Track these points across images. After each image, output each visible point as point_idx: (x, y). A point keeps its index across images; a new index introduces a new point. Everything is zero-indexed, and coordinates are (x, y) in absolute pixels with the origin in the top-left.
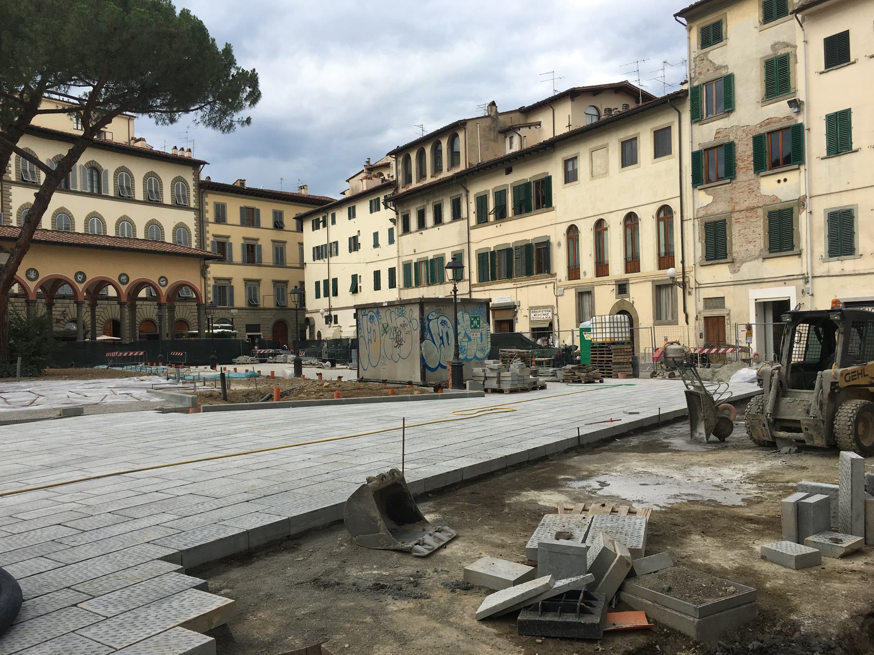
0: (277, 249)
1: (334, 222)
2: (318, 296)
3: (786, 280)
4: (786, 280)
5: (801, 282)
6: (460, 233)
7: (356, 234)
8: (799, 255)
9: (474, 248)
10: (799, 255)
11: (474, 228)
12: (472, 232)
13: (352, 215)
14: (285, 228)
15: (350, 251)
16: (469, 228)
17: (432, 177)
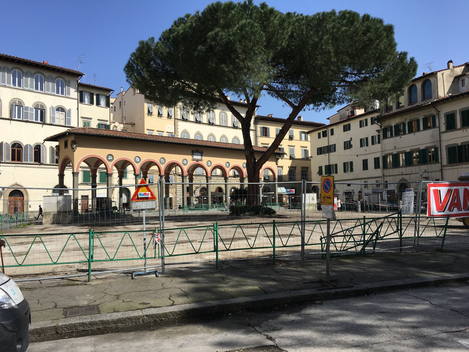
0: (291, 149)
1: (332, 134)
2: (345, 171)
6: (432, 136)
7: (350, 140)
9: (444, 144)
11: (444, 132)
12: (443, 135)
13: (347, 128)
14: (294, 139)
15: (318, 154)
16: (440, 133)
17: (408, 105)
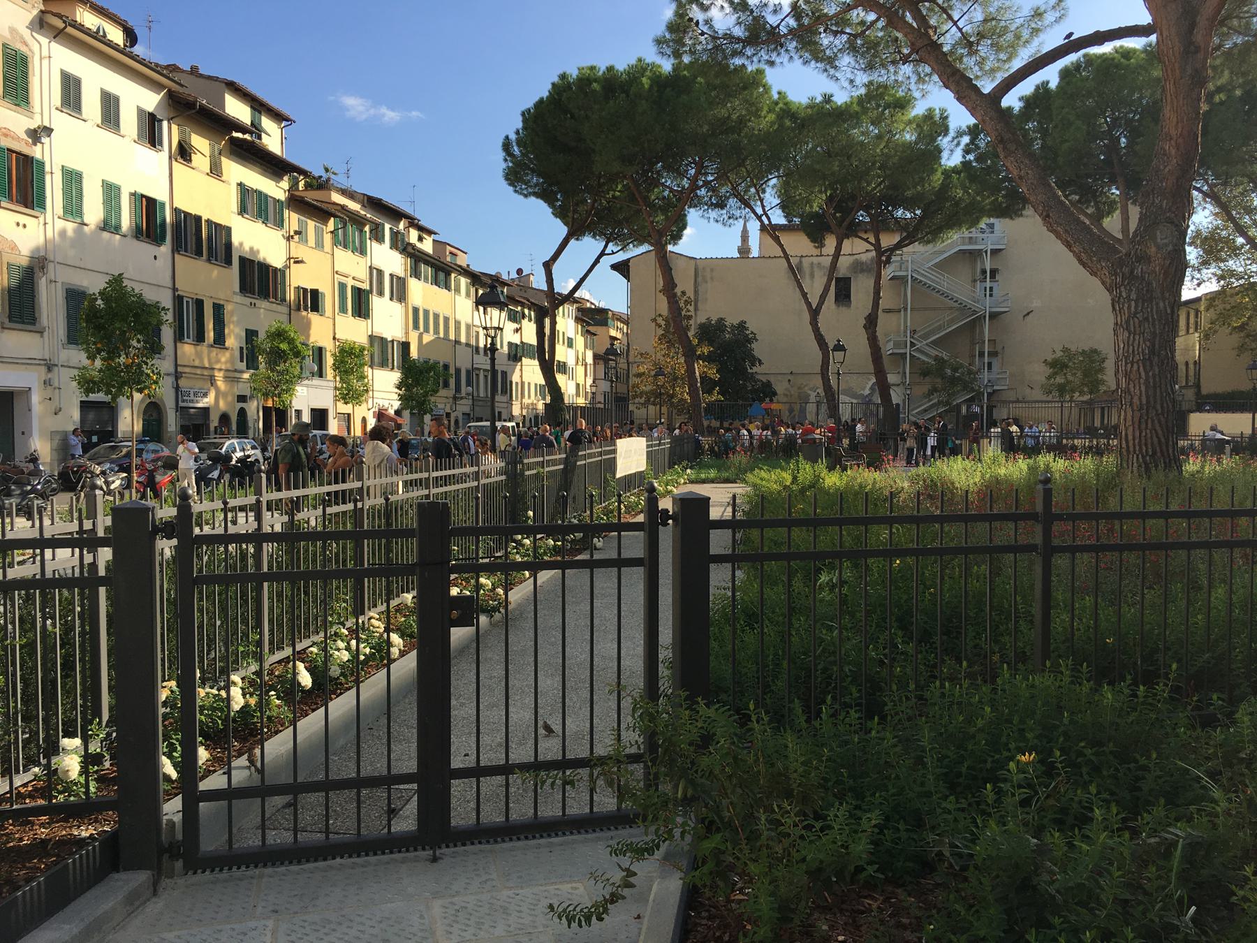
3: (28, 362)
4: (28, 362)
5: (43, 369)
8: (41, 333)
10: (41, 333)
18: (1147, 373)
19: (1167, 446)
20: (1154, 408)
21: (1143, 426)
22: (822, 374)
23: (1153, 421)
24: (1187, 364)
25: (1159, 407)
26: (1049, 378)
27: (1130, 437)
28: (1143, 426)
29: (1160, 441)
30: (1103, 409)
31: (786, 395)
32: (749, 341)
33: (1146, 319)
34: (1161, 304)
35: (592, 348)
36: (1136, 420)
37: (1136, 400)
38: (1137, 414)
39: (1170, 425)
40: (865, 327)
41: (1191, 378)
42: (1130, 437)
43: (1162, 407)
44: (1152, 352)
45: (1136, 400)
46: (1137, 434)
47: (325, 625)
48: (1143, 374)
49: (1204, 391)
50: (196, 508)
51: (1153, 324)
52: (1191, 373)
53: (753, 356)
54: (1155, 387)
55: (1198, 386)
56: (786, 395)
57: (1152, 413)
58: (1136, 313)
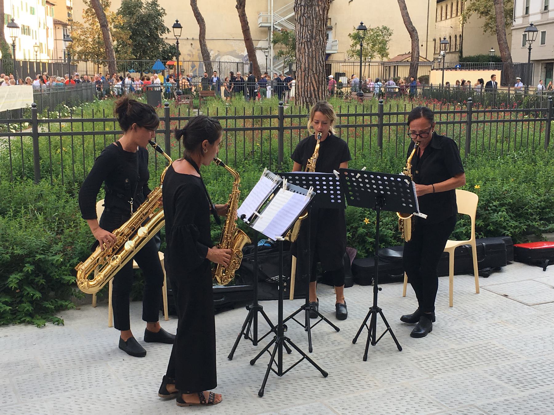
18: (308, 49)
19: (318, 91)
20: (312, 70)
21: (306, 80)
22: (200, 41)
23: (311, 78)
24: (456, 36)
25: (314, 70)
26: (353, 46)
27: (300, 87)
28: (306, 80)
29: (314, 89)
30: (395, 66)
31: (189, 55)
32: (160, 14)
33: (309, 17)
34: (317, 9)
35: (52, 15)
36: (303, 76)
37: (303, 66)
38: (303, 73)
39: (321, 79)
40: (237, 7)
41: (458, 46)
42: (300, 87)
43: (316, 69)
44: (312, 37)
45: (303, 66)
46: (303, 85)
47: (33, 318)
48: (307, 49)
49: (464, 55)
50: (74, 203)
51: (313, 20)
52: (458, 42)
53: (163, 26)
54: (312, 57)
55: (461, 52)
56: (189, 55)
57: (311, 73)
58: (304, 14)
